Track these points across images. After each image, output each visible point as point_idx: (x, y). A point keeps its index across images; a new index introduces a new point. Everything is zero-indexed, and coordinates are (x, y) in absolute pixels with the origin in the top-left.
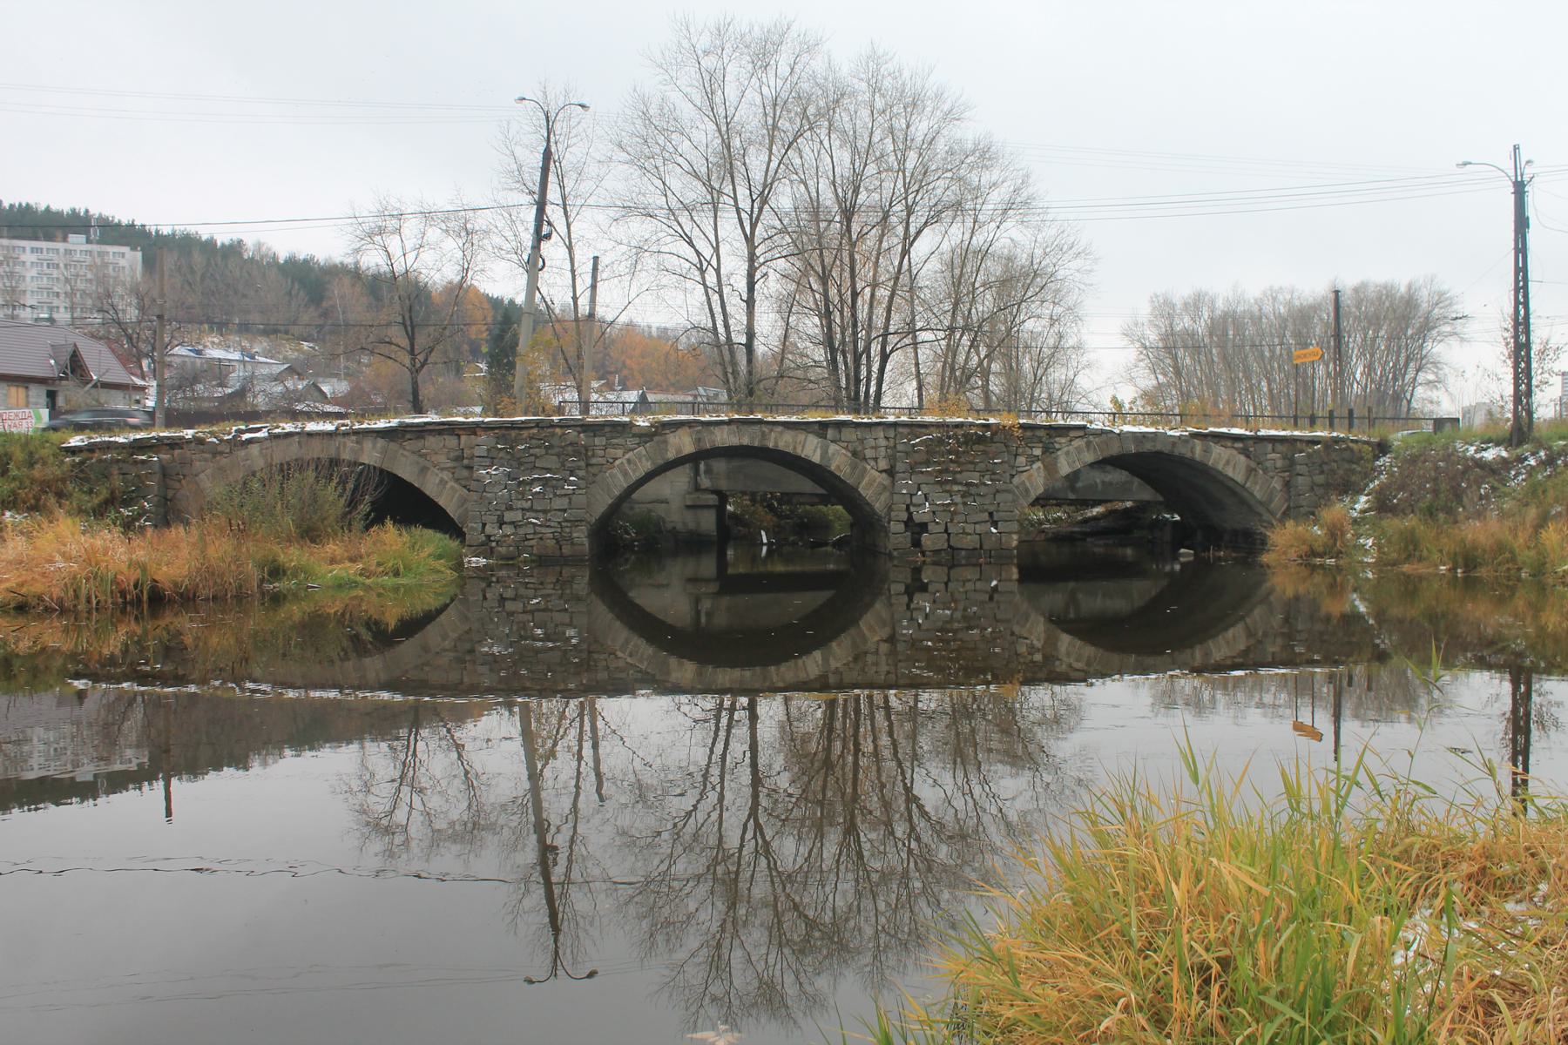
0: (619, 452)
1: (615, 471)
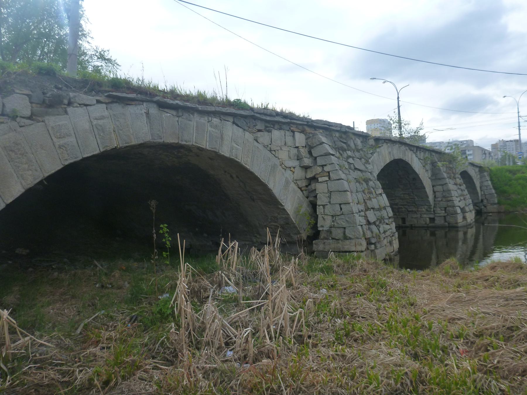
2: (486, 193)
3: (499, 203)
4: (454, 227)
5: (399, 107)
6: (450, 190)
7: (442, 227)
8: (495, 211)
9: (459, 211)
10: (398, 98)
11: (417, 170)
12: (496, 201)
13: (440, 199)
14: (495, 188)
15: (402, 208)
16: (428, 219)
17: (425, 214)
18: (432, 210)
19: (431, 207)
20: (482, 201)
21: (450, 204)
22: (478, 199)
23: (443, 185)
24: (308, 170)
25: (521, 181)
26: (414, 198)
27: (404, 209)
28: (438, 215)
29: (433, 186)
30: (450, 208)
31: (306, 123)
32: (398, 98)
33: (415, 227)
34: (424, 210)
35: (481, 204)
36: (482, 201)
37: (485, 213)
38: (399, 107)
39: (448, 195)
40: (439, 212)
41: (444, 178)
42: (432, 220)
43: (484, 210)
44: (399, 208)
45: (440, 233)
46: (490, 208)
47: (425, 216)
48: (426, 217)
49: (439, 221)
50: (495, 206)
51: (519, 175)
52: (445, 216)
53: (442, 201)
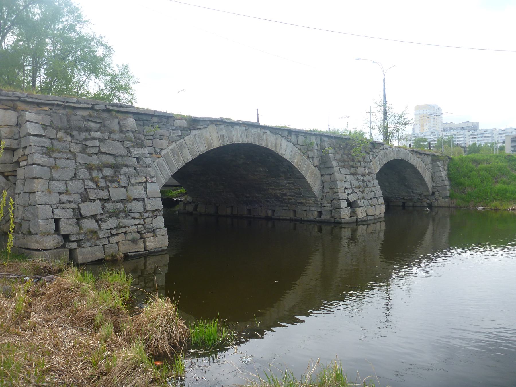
0: (165, 143)
1: (161, 160)
2: (438, 185)
3: (451, 197)
4: (337, 224)
5: (384, 89)
6: (336, 181)
7: (328, 223)
8: (447, 205)
9: (344, 204)
10: (384, 80)
11: (287, 156)
12: (448, 194)
13: (327, 191)
14: (450, 179)
15: (291, 199)
16: (316, 212)
17: (313, 207)
18: (320, 203)
19: (434, 199)
20: (433, 193)
21: (335, 196)
22: (428, 191)
23: (330, 175)
24: (15, 152)
25: (482, 173)
26: (299, 189)
27: (293, 200)
28: (324, 208)
29: (322, 176)
30: (335, 201)
31: (17, 99)
32: (384, 80)
33: (304, 221)
34: (311, 202)
35: (432, 197)
36: (433, 193)
37: (436, 207)
38: (384, 89)
39: (334, 187)
40: (325, 205)
41: (332, 167)
42: (320, 213)
43: (435, 204)
44: (289, 199)
45: (326, 228)
46: (442, 202)
47: (313, 209)
48: (315, 211)
49: (326, 216)
50: (447, 200)
51: (482, 166)
52: (331, 210)
53: (329, 193)
